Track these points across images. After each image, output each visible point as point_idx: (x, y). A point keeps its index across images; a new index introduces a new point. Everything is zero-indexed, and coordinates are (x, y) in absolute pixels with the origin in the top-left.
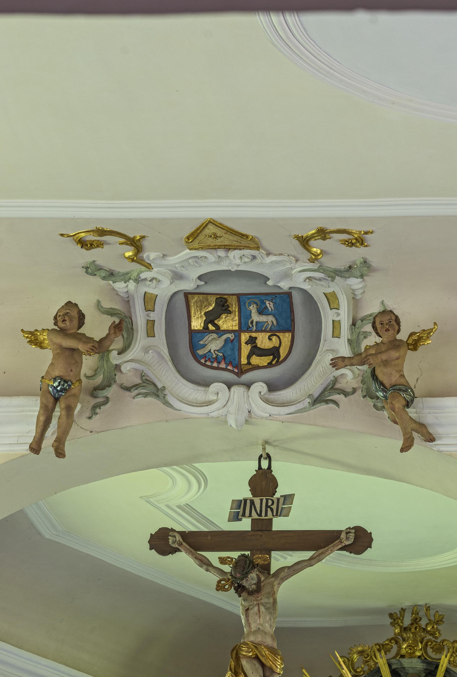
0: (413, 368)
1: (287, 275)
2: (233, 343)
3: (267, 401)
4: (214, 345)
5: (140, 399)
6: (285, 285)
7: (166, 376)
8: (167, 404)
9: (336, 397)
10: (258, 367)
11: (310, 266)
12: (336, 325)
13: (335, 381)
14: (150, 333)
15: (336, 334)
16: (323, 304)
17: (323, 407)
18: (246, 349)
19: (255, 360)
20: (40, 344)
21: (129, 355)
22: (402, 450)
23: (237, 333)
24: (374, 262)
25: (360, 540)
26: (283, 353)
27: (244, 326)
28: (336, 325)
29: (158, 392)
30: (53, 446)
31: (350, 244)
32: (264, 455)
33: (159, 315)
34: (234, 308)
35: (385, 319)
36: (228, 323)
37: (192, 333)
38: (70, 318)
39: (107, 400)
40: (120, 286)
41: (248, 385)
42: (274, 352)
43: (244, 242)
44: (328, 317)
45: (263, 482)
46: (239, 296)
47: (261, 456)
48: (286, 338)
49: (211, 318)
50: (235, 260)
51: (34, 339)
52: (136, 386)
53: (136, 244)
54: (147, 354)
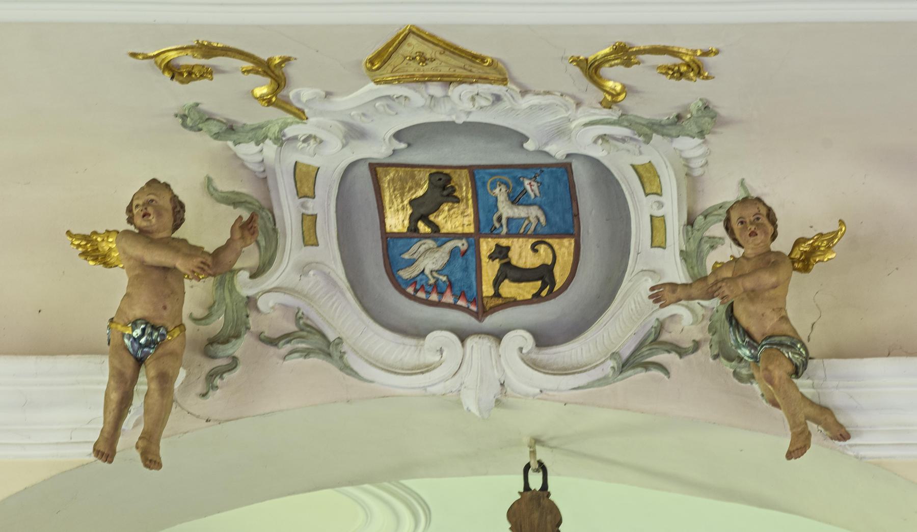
0: (804, 304)
1: (560, 132)
2: (465, 258)
3: (534, 365)
4: (430, 260)
5: (296, 361)
6: (558, 151)
7: (343, 317)
8: (347, 369)
9: (662, 357)
10: (513, 303)
11: (604, 114)
12: (657, 224)
13: (661, 327)
14: (309, 238)
15: (658, 240)
16: (630, 185)
17: (640, 375)
18: (490, 270)
19: (509, 289)
20: (103, 259)
21: (272, 279)
22: (790, 455)
23: (474, 239)
24: (724, 108)
26: (560, 275)
27: (486, 225)
28: (657, 224)
29: (330, 349)
30: (137, 448)
31: (677, 74)
32: (534, 465)
33: (324, 204)
34: (465, 191)
35: (749, 213)
36: (455, 219)
37: (388, 238)
38: (157, 212)
39: (234, 363)
40: (248, 151)
41: (498, 336)
42: (544, 274)
43: (477, 70)
44: (641, 209)
46: (472, 170)
47: (527, 468)
48: (564, 248)
49: (422, 211)
50: (462, 103)
51: (91, 250)
52: (288, 337)
53: (274, 72)
54: (305, 276)
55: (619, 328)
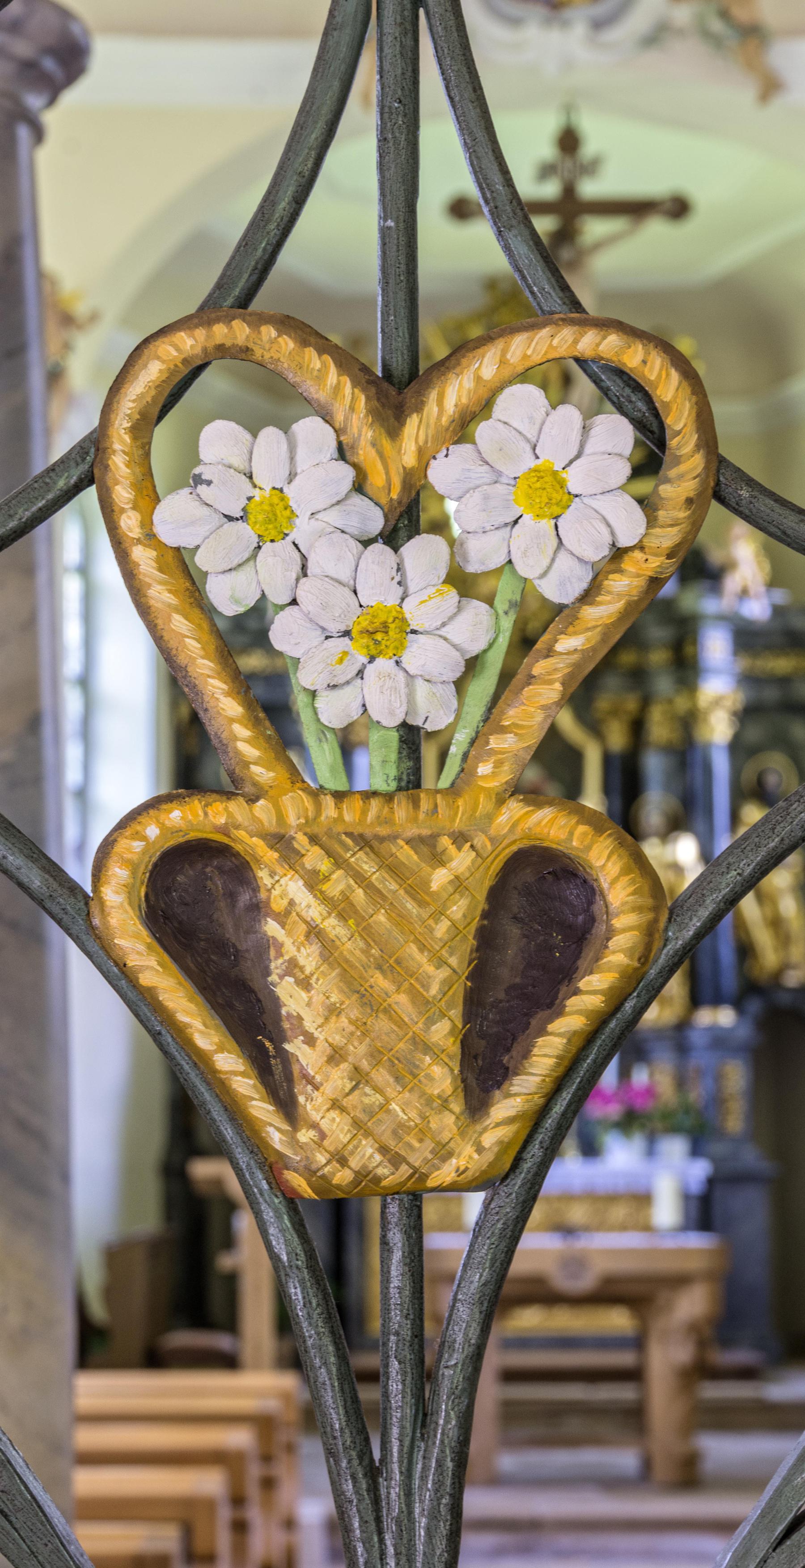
25: (678, 208)
45: (569, 141)
55: (638, 22)
